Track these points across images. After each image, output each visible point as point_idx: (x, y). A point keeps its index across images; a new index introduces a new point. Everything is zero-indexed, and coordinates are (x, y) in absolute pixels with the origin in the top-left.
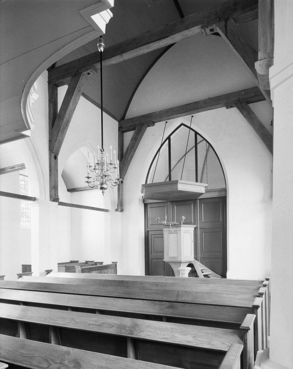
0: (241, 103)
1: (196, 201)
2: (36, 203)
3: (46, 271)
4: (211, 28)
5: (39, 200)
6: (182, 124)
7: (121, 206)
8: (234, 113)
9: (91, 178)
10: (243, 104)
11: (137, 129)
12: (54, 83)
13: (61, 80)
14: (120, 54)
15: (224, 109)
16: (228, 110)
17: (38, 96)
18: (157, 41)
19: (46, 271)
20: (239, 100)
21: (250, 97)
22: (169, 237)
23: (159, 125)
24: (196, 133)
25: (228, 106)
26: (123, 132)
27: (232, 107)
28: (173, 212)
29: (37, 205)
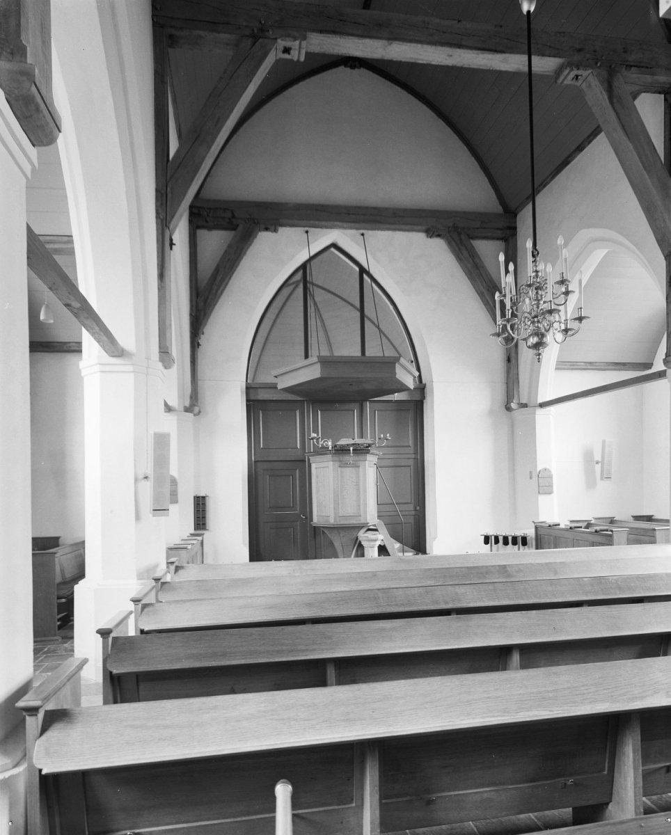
0: (459, 234)
1: (364, 404)
2: (127, 363)
3: (632, 516)
4: (286, 56)
5: (134, 355)
6: (334, 245)
7: (194, 403)
8: (437, 252)
9: (588, 318)
10: (463, 237)
11: (240, 228)
12: (173, 32)
13: (201, 33)
14: (389, 39)
15: (422, 236)
16: (429, 240)
17: (302, 59)
18: (477, 52)
19: (632, 516)
20: (455, 228)
21: (473, 228)
22: (324, 474)
23: (289, 235)
24: (363, 271)
25: (431, 233)
26: (198, 227)
27: (439, 236)
28: (315, 421)
29: (130, 368)
